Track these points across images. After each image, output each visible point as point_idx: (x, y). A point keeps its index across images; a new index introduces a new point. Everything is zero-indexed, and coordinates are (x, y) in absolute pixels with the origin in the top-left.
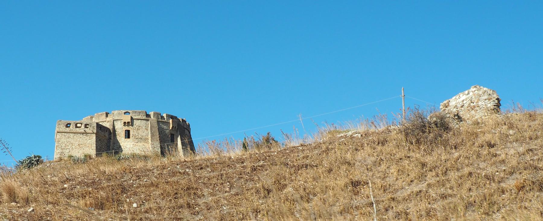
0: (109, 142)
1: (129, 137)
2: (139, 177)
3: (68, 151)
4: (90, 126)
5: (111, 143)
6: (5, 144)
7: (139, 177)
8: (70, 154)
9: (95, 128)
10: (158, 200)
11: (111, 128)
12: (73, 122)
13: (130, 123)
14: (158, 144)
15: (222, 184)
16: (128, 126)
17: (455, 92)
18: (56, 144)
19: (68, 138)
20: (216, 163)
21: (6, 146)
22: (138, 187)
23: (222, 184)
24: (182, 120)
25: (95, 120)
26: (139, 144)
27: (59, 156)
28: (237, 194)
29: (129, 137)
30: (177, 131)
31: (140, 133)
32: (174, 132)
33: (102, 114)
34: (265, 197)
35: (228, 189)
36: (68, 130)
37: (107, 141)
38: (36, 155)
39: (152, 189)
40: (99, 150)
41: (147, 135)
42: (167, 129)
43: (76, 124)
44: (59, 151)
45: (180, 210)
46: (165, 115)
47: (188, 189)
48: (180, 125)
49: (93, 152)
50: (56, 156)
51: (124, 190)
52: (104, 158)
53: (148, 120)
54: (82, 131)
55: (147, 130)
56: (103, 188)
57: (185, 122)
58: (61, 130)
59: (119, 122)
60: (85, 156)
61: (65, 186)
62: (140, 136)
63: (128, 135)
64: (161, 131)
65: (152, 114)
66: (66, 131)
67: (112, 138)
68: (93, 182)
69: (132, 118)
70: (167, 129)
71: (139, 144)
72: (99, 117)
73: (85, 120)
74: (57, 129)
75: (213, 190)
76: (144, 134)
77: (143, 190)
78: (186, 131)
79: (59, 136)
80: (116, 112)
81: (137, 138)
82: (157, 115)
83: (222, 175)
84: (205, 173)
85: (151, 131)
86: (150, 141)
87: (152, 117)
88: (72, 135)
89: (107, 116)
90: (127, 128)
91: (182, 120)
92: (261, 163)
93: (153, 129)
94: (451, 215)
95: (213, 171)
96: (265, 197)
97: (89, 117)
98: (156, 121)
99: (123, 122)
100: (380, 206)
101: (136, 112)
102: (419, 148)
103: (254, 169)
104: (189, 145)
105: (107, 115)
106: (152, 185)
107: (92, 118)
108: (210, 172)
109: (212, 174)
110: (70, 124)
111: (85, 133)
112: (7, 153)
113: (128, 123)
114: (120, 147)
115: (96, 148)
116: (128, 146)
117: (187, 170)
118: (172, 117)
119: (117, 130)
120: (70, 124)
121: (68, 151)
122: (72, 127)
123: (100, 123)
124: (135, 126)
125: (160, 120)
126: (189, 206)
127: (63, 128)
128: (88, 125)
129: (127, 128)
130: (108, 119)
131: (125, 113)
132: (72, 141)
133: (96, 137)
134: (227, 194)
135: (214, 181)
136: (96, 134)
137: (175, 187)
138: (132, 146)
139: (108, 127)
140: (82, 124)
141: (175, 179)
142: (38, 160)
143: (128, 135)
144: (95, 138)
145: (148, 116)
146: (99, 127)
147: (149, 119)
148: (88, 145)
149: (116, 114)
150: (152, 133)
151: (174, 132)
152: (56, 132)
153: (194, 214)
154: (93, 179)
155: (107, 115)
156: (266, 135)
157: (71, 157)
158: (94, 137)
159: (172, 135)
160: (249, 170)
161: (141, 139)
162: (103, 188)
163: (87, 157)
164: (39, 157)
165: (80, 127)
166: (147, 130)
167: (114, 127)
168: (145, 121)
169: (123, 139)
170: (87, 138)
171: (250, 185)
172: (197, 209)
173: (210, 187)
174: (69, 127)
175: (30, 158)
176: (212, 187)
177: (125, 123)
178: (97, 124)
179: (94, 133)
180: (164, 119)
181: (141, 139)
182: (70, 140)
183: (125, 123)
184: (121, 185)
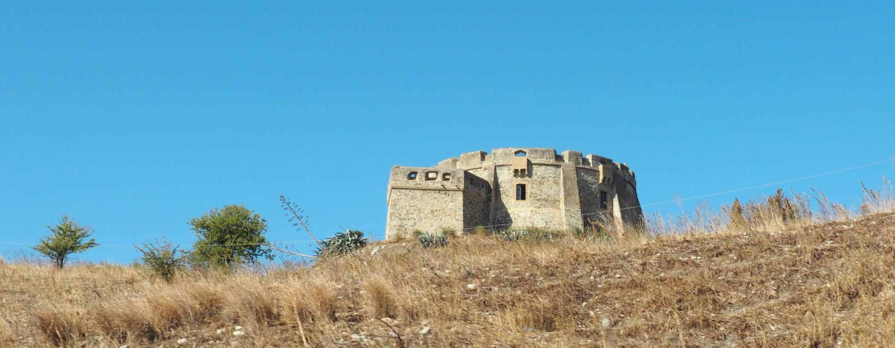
0: (488, 206)
1: (523, 198)
2: (605, 270)
3: (412, 222)
4: (453, 178)
5: (492, 209)
6: (296, 210)
7: (605, 270)
8: (416, 228)
9: (463, 180)
10: (648, 314)
11: (490, 180)
12: (420, 170)
13: (527, 172)
14: (577, 209)
15: (762, 282)
16: (522, 176)
18: (389, 211)
20: (746, 245)
22: (605, 290)
23: (762, 282)
24: (622, 165)
25: (461, 166)
26: (542, 210)
27: (395, 232)
28: (792, 302)
29: (523, 198)
30: (612, 187)
32: (607, 190)
33: (473, 156)
34: (844, 307)
35: (773, 293)
36: (411, 183)
37: (484, 206)
38: (353, 230)
39: (634, 292)
40: (470, 223)
42: (594, 183)
43: (427, 174)
44: (396, 222)
45: (692, 331)
46: (589, 157)
47: (701, 292)
48: (618, 175)
49: (457, 224)
50: (390, 233)
51: (581, 295)
52: (480, 237)
53: (558, 166)
54: (439, 186)
55: (557, 184)
56: (541, 291)
57: (627, 169)
58: (399, 184)
59: (505, 169)
60: (445, 233)
61: (471, 286)
63: (521, 192)
64: (583, 187)
65: (565, 154)
66: (408, 185)
67: (493, 199)
68: (520, 280)
69: (529, 163)
70: (594, 183)
71: (543, 210)
72: (468, 159)
73: (443, 166)
74: (391, 183)
75: (746, 293)
76: (552, 192)
77: (617, 295)
78: (628, 186)
79: (395, 195)
80: (500, 151)
81: (539, 200)
82: (577, 157)
83: (759, 266)
84: (726, 263)
85: (565, 187)
86: (562, 205)
87: (566, 160)
88: (419, 193)
89: (483, 158)
90: (520, 181)
91: (622, 165)
92: (829, 244)
93: (569, 183)
95: (741, 258)
96: (844, 307)
97: (450, 160)
98: (573, 169)
99: (512, 169)
101: (536, 151)
102: (196, 298)
103: (817, 256)
104: (633, 215)
105: (483, 156)
106: (634, 284)
107: (455, 161)
108: (736, 261)
109: (741, 265)
110: (416, 173)
111: (444, 190)
112: (299, 226)
113: (523, 171)
114: (507, 215)
115: (464, 217)
116: (522, 214)
117: (693, 257)
118: (603, 161)
119: (502, 185)
120: (416, 173)
121: (412, 222)
122: (419, 179)
123: (471, 172)
124: (534, 177)
125: (582, 167)
126: (707, 324)
127: (403, 181)
128: (449, 174)
129: (520, 181)
130: (485, 164)
131: (516, 153)
132: (420, 205)
133: (464, 197)
134: (772, 302)
135: (747, 277)
136: (464, 192)
137: (675, 288)
138: (529, 213)
139: (486, 179)
140: (437, 173)
141: (674, 273)
142: (359, 242)
143: (521, 192)
145: (559, 158)
146: (470, 179)
147: (561, 163)
148: (447, 213)
149: (499, 155)
150: (565, 191)
151: (607, 190)
152: (389, 187)
153: (718, 339)
154: (518, 273)
155: (483, 156)
157: (418, 233)
158: (460, 197)
160: (808, 257)
161: (546, 201)
162: (541, 291)
163: (446, 239)
164: (360, 235)
165: (434, 179)
166: (557, 184)
167: (496, 178)
168: (553, 168)
169: (513, 200)
170: (446, 199)
171: (814, 284)
172: (722, 329)
173: (740, 288)
174: (414, 178)
175: (343, 236)
176: (743, 288)
177: (516, 171)
178: (466, 173)
179: (459, 190)
180: (589, 164)
181: (546, 201)
182: (416, 202)
183: (516, 171)
184: (575, 286)
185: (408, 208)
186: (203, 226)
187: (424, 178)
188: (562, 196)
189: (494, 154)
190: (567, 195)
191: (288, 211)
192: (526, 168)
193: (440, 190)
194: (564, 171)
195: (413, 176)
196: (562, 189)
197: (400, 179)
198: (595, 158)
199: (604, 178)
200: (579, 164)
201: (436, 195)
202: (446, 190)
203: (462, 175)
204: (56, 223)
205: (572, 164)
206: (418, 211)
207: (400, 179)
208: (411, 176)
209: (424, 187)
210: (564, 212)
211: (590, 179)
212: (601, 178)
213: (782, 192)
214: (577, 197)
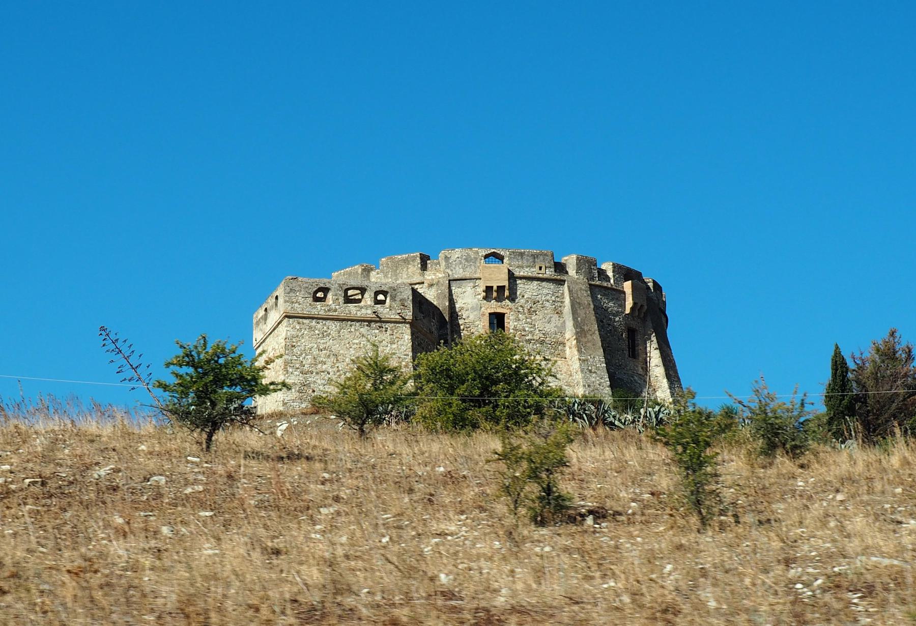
4: (393, 299)
9: (410, 304)
11: (442, 304)
14: (598, 359)
16: (499, 299)
21: (134, 361)
30: (644, 320)
31: (539, 324)
33: (406, 261)
41: (561, 330)
42: (617, 314)
46: (607, 267)
53: (561, 282)
54: (368, 313)
55: (560, 313)
58: (298, 309)
59: (468, 287)
62: (538, 335)
64: (603, 318)
65: (570, 261)
66: (314, 312)
70: (617, 314)
72: (396, 267)
76: (550, 328)
80: (456, 254)
82: (588, 265)
87: (572, 271)
88: (333, 326)
89: (424, 267)
90: (494, 307)
91: (654, 282)
93: (581, 312)
94: (636, 562)
97: (359, 269)
101: (522, 254)
105: (424, 261)
107: (367, 271)
110: (326, 290)
111: (378, 321)
113: (501, 289)
118: (626, 273)
120: (326, 290)
124: (521, 301)
127: (304, 305)
128: (385, 293)
129: (494, 307)
130: (429, 276)
131: (486, 257)
132: (336, 348)
133: (412, 334)
136: (413, 325)
144: (407, 337)
145: (560, 268)
150: (577, 325)
155: (424, 261)
159: (632, 332)
167: (452, 302)
168: (552, 286)
179: (404, 321)
180: (607, 279)
183: (489, 289)
185: (315, 352)
187: (341, 300)
188: (569, 333)
189: (447, 258)
190: (580, 334)
191: (112, 356)
192: (506, 283)
193: (370, 322)
194: (570, 291)
196: (570, 324)
197: (301, 300)
198: (617, 268)
199: (635, 304)
200: (592, 278)
201: (363, 330)
203: (408, 294)
204: (881, 336)
205: (582, 279)
206: (332, 359)
207: (301, 300)
209: (343, 316)
210: (576, 365)
211: (611, 305)
213: (897, 334)
214: (597, 338)
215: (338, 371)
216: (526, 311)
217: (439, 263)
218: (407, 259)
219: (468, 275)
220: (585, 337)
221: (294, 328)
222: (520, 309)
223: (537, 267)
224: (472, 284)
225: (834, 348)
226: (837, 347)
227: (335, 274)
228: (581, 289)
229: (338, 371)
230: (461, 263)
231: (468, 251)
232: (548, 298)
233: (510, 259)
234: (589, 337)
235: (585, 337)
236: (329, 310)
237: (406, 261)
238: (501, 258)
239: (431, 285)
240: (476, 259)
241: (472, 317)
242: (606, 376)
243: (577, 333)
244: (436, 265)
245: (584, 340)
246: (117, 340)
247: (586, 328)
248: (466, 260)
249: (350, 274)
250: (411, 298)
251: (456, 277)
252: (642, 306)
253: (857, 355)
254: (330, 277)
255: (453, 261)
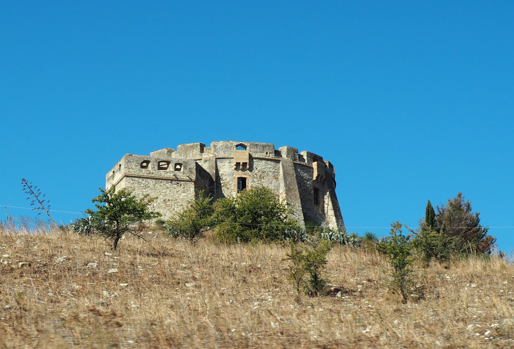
4: (185, 168)
9: (194, 171)
11: (212, 172)
16: (244, 170)
17: (281, 147)
19: (146, 187)
21: (41, 198)
30: (323, 184)
33: (192, 147)
36: (144, 172)
41: (278, 188)
42: (308, 180)
46: (304, 154)
53: (278, 162)
54: (171, 175)
55: (277, 179)
58: (132, 172)
59: (226, 162)
64: (301, 182)
65: (284, 150)
69: (251, 158)
70: (308, 180)
72: (186, 150)
80: (220, 144)
82: (293, 152)
85: (285, 182)
87: (284, 155)
88: (151, 182)
89: (202, 151)
90: (240, 174)
91: (329, 163)
93: (289, 179)
100: (52, 279)
101: (257, 145)
105: (202, 147)
107: (170, 152)
110: (148, 162)
111: (176, 180)
113: (245, 164)
118: (314, 157)
120: (148, 162)
127: (135, 170)
128: (180, 165)
129: (240, 174)
130: (205, 156)
131: (237, 146)
136: (195, 183)
144: (192, 189)
145: (278, 153)
150: (286, 185)
155: (202, 147)
156: (456, 196)
159: (316, 190)
167: (217, 171)
168: (273, 163)
179: (191, 180)
180: (304, 160)
183: (238, 164)
186: (457, 207)
187: (156, 168)
189: (215, 146)
192: (248, 161)
193: (172, 180)
194: (283, 167)
195: (145, 164)
197: (134, 167)
198: (309, 154)
199: (318, 175)
200: (295, 160)
201: (168, 185)
202: (178, 180)
203: (193, 165)
204: (453, 197)
205: (290, 160)
207: (134, 167)
208: (144, 164)
212: (315, 174)
213: (462, 196)
214: (297, 193)
215: (154, 207)
216: (258, 177)
217: (210, 149)
218: (192, 146)
219: (226, 156)
220: (291, 192)
221: (130, 182)
222: (255, 176)
223: (265, 153)
224: (228, 161)
225: (427, 202)
226: (429, 202)
227: (152, 153)
228: (289, 166)
229: (154, 207)
230: (223, 149)
231: (227, 143)
232: (271, 170)
233: (250, 147)
234: (293, 192)
235: (291, 192)
236: (149, 173)
237: (192, 147)
238: (245, 147)
239: (206, 161)
240: (231, 147)
241: (228, 179)
242: (302, 214)
243: (286, 190)
244: (209, 149)
245: (290, 194)
246: (31, 186)
247: (291, 187)
248: (226, 147)
249: (160, 153)
250: (195, 168)
251: (220, 156)
252: (322, 176)
253: (440, 207)
254: (149, 155)
255: (219, 147)
